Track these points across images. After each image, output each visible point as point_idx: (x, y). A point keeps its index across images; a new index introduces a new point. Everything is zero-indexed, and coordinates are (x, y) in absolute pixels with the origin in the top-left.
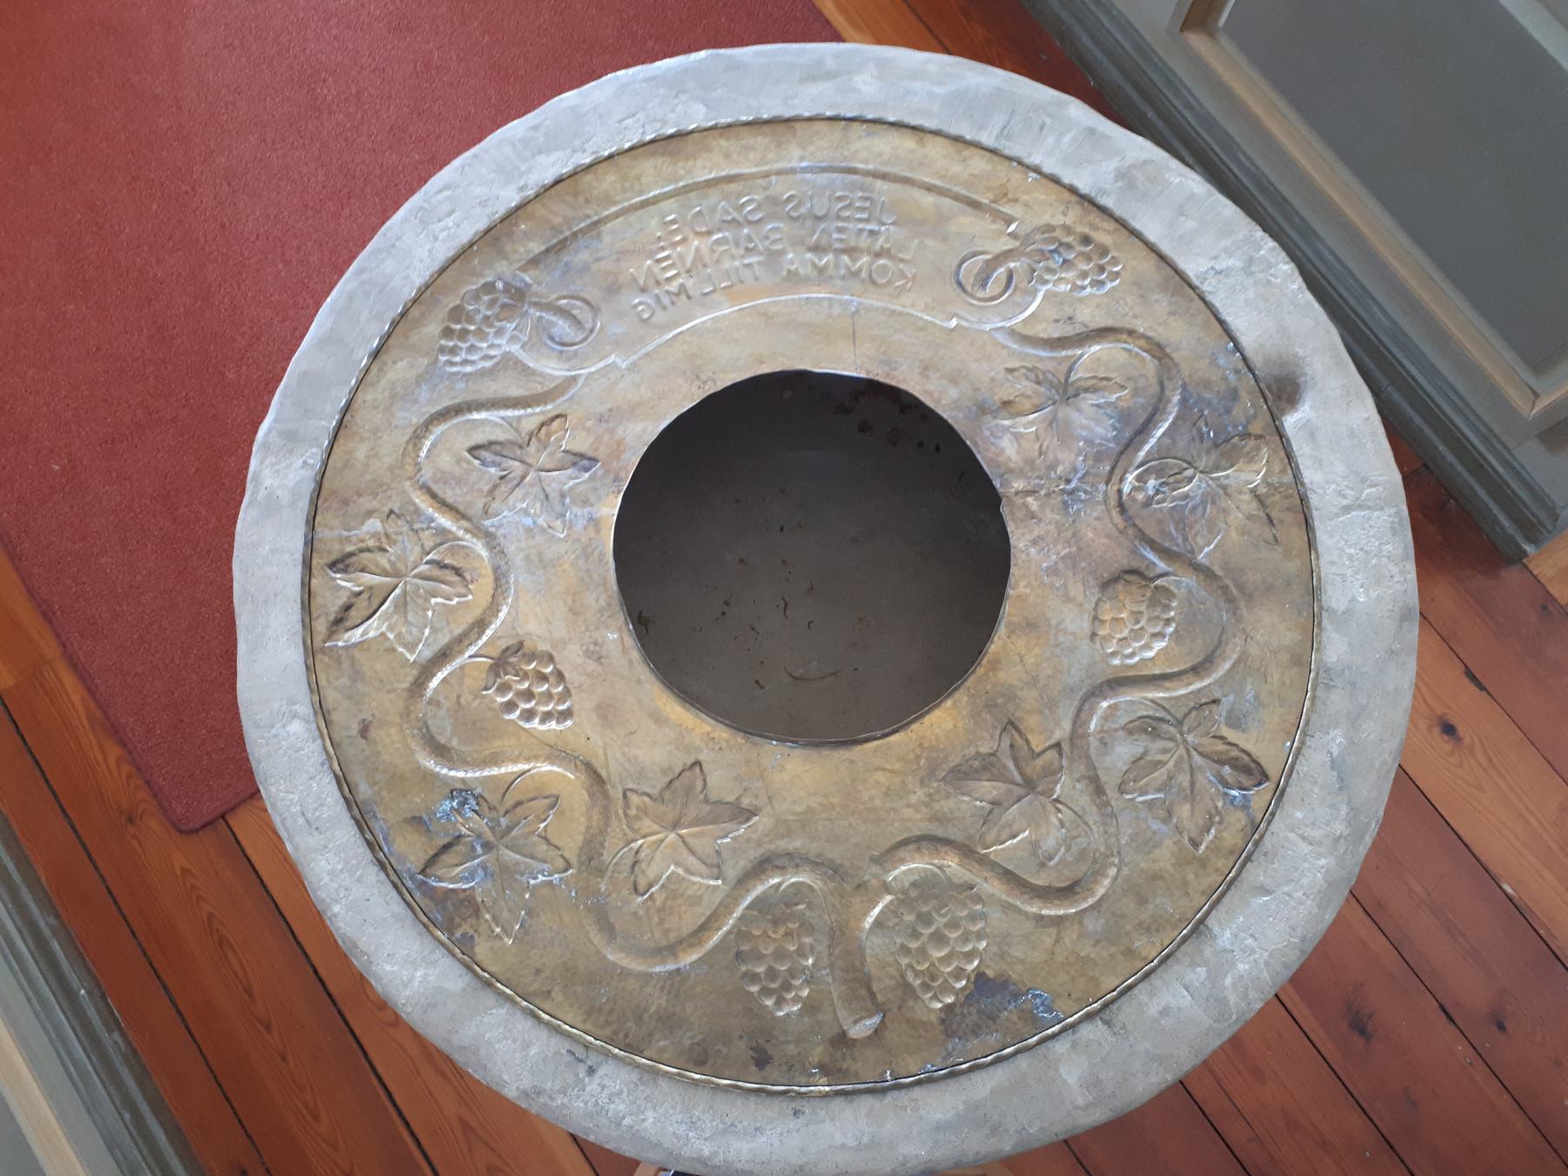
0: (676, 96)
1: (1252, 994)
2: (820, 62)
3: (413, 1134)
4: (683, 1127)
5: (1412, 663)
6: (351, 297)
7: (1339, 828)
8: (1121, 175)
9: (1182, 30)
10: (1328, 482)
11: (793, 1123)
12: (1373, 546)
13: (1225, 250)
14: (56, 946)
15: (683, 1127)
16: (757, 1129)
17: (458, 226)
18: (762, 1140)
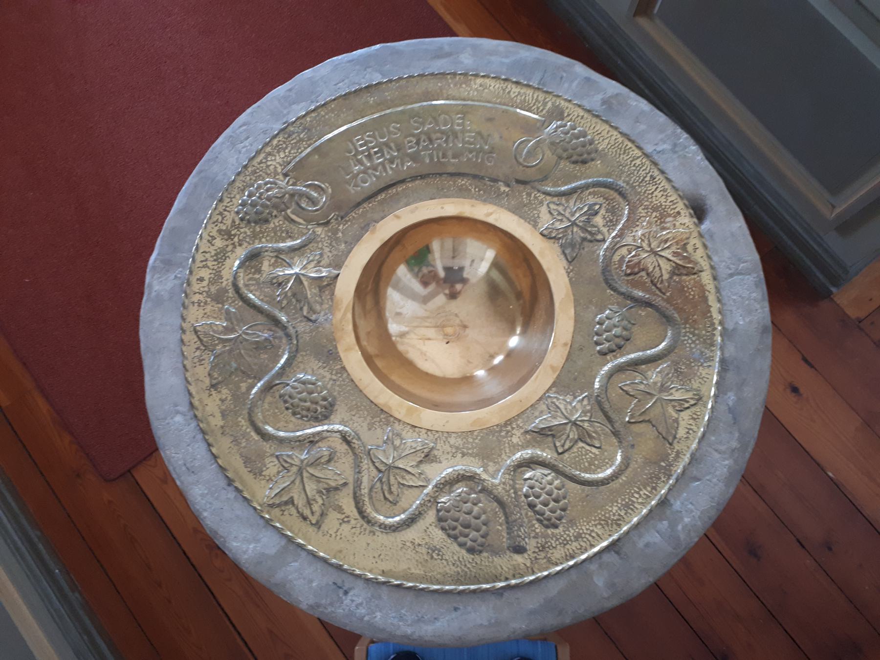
0: (365, 70)
1: (693, 534)
2: (441, 48)
3: (243, 639)
4: (396, 620)
5: (769, 354)
6: (196, 186)
7: (734, 444)
8: (604, 102)
9: (634, 15)
10: (721, 261)
11: (454, 615)
12: (745, 294)
13: (661, 140)
14: (40, 546)
15: (396, 620)
16: (435, 619)
17: (251, 145)
18: (438, 624)
